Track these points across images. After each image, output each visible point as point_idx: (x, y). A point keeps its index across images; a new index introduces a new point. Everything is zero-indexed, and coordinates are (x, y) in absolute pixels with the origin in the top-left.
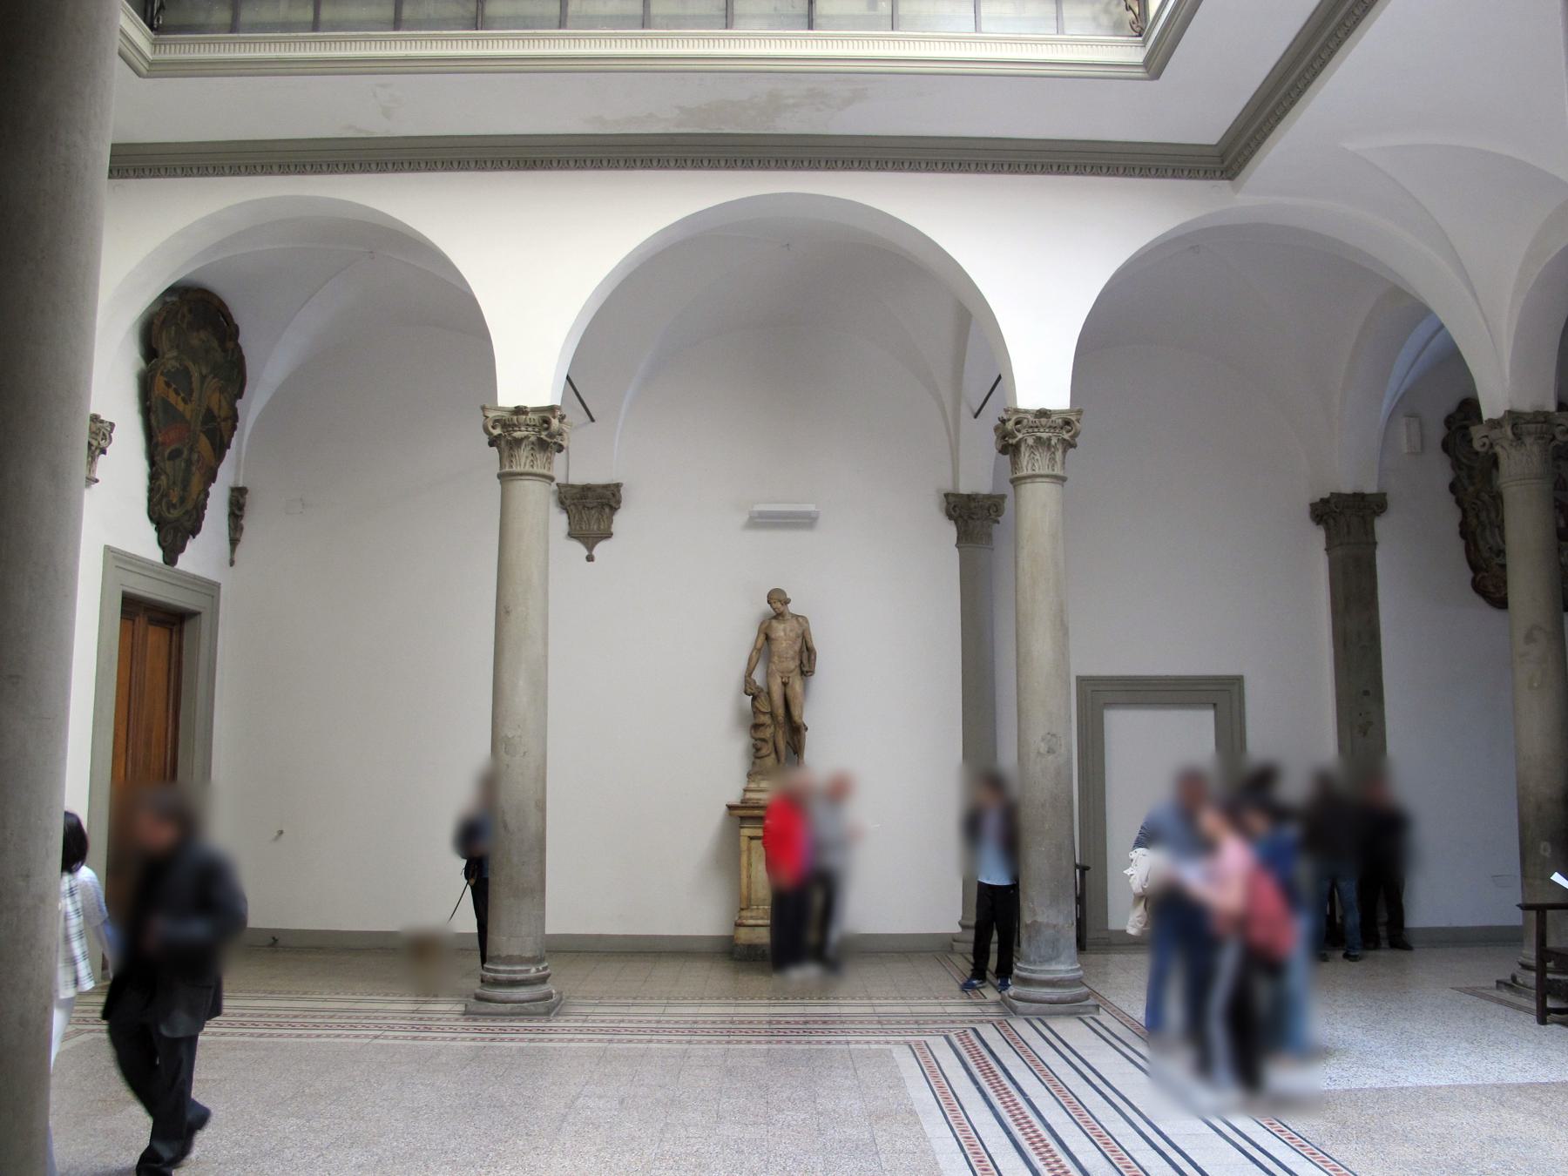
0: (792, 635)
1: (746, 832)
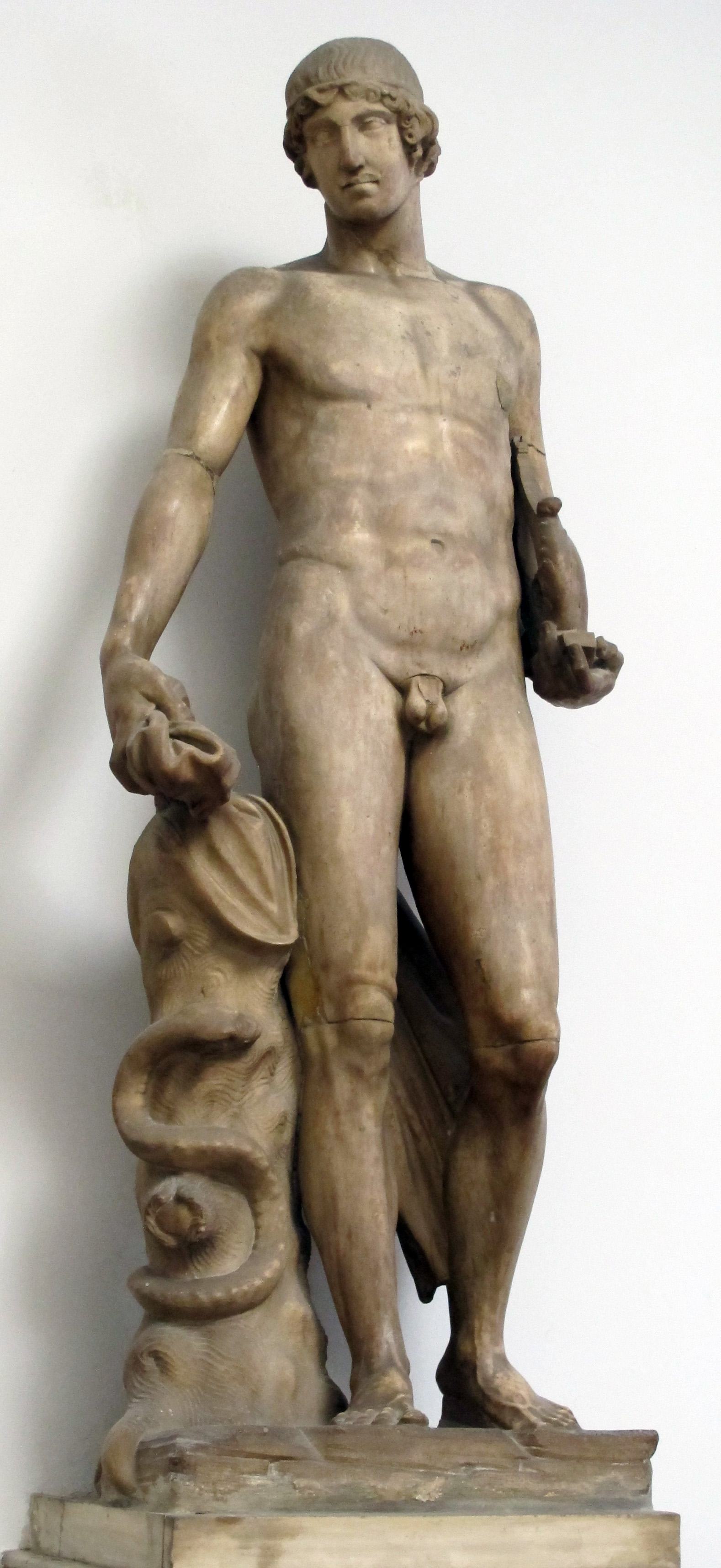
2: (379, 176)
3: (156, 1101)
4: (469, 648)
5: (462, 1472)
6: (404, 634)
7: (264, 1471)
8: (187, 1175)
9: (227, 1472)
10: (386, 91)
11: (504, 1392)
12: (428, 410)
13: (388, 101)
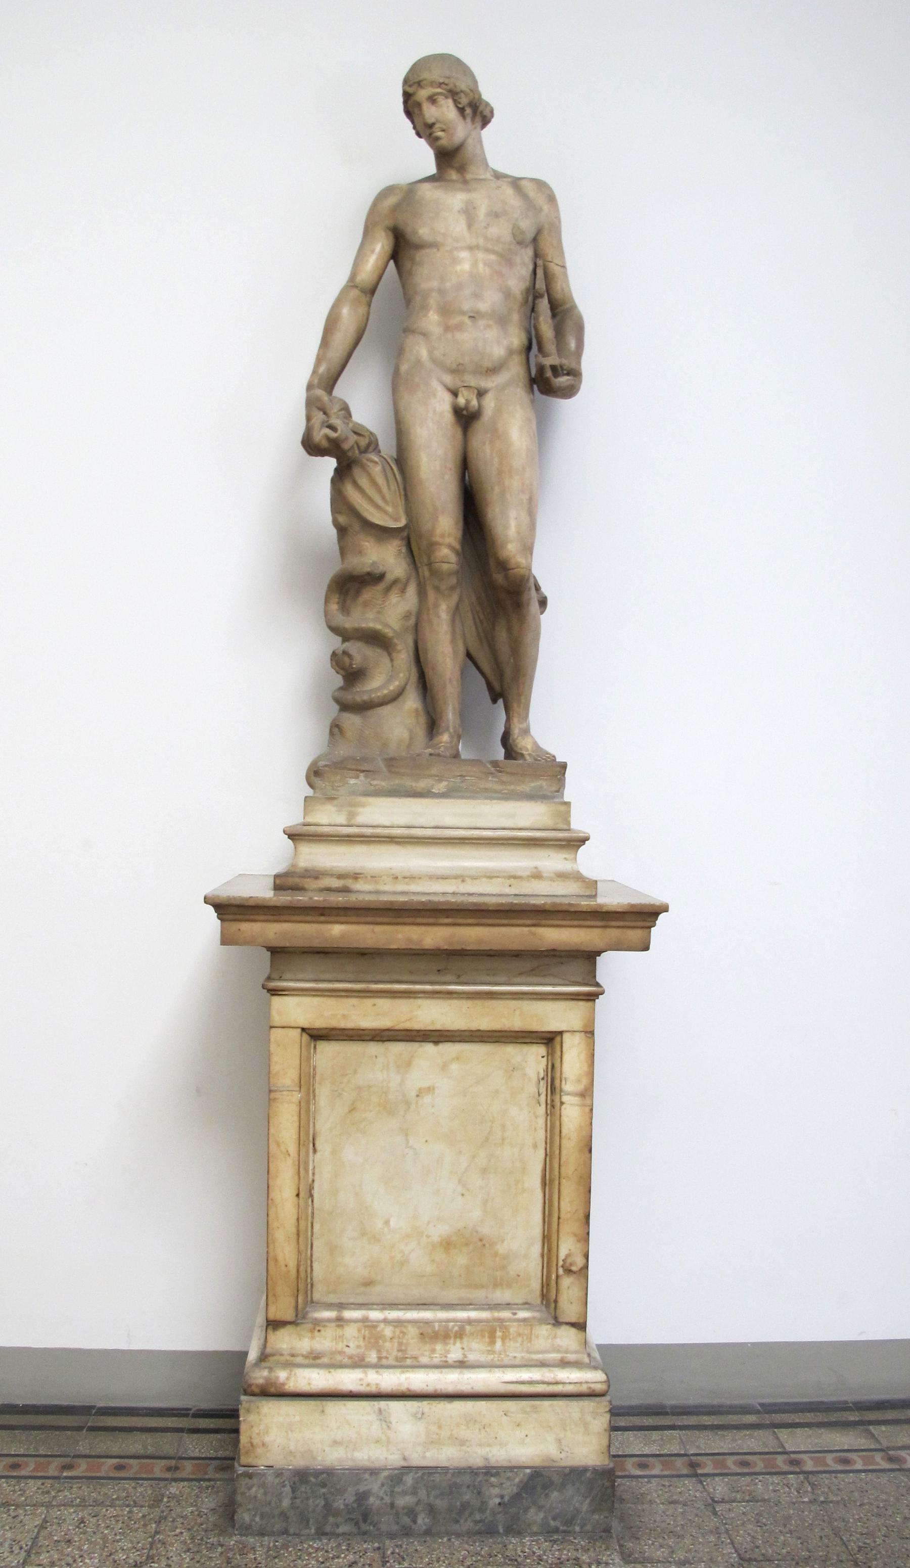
0: (501, 231)
1: (297, 1009)
2: (444, 127)
3: (345, 609)
4: (493, 370)
5: (458, 780)
6: (454, 366)
7: (357, 777)
8: (352, 641)
9: (339, 777)
10: (441, 81)
11: (519, 746)
12: (471, 248)
13: (443, 86)
